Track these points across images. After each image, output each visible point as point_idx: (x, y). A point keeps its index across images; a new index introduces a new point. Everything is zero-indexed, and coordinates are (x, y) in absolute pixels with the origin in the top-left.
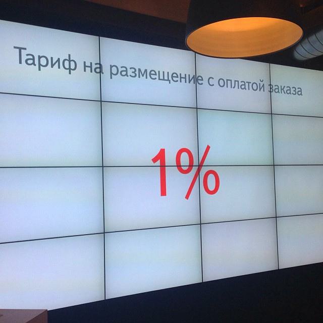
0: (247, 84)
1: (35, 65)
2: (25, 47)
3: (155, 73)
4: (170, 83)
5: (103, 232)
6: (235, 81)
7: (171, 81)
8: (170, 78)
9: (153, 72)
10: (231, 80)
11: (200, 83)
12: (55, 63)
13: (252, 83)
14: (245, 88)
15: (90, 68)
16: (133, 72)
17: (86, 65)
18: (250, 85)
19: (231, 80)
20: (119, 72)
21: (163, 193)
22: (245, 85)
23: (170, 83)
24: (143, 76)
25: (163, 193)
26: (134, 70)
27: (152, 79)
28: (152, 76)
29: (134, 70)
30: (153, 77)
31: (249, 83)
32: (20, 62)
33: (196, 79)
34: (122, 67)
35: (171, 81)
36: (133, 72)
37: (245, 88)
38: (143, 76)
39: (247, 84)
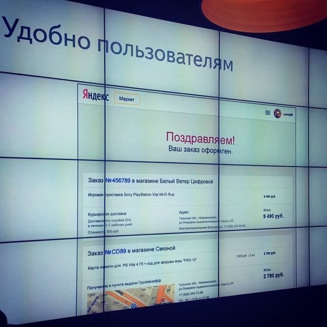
0: (186, 58)
1: (185, 64)
2: (15, 20)
3: (201, 58)
4: (31, 43)
5: (308, 168)
6: (127, 45)
7: (34, 40)
8: (32, 36)
9: (198, 58)
10: (132, 46)
11: (198, 64)
12: (229, 65)
13: (194, 56)
14: (183, 62)
15: (72, 42)
16: (149, 53)
17: (72, 42)
18: (192, 58)
19: (132, 46)
20: (176, 60)
21: (167, 140)
22: (183, 58)
23: (31, 43)
24: (228, 68)
25: (167, 140)
26: (150, 51)
27: (197, 65)
28: (197, 62)
29: (150, 51)
30: (198, 63)
31: (190, 55)
32: (211, 67)
33: (219, 64)
34: (179, 53)
35: (34, 40)
36: (149, 53)
37: (183, 62)
38: (228, 68)
39: (186, 58)
